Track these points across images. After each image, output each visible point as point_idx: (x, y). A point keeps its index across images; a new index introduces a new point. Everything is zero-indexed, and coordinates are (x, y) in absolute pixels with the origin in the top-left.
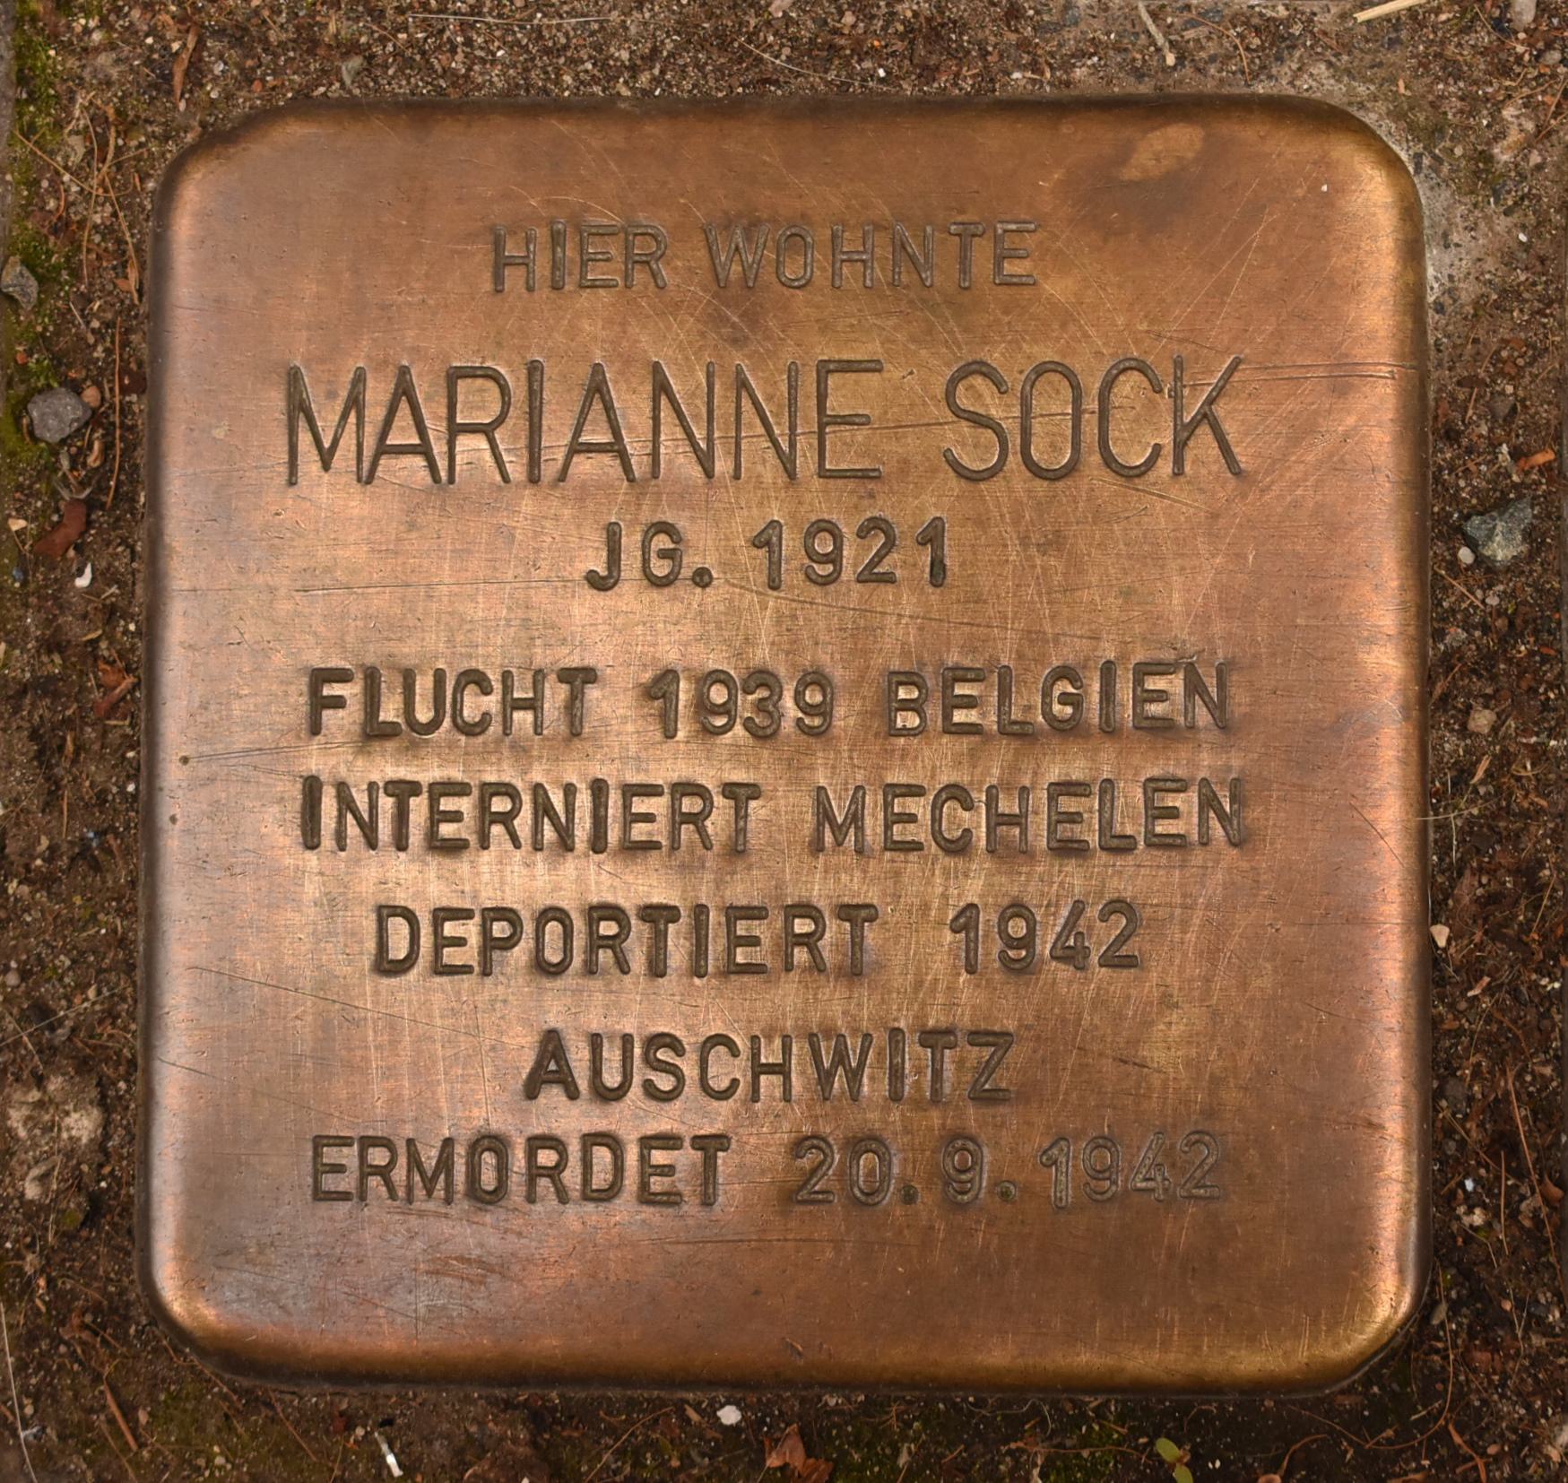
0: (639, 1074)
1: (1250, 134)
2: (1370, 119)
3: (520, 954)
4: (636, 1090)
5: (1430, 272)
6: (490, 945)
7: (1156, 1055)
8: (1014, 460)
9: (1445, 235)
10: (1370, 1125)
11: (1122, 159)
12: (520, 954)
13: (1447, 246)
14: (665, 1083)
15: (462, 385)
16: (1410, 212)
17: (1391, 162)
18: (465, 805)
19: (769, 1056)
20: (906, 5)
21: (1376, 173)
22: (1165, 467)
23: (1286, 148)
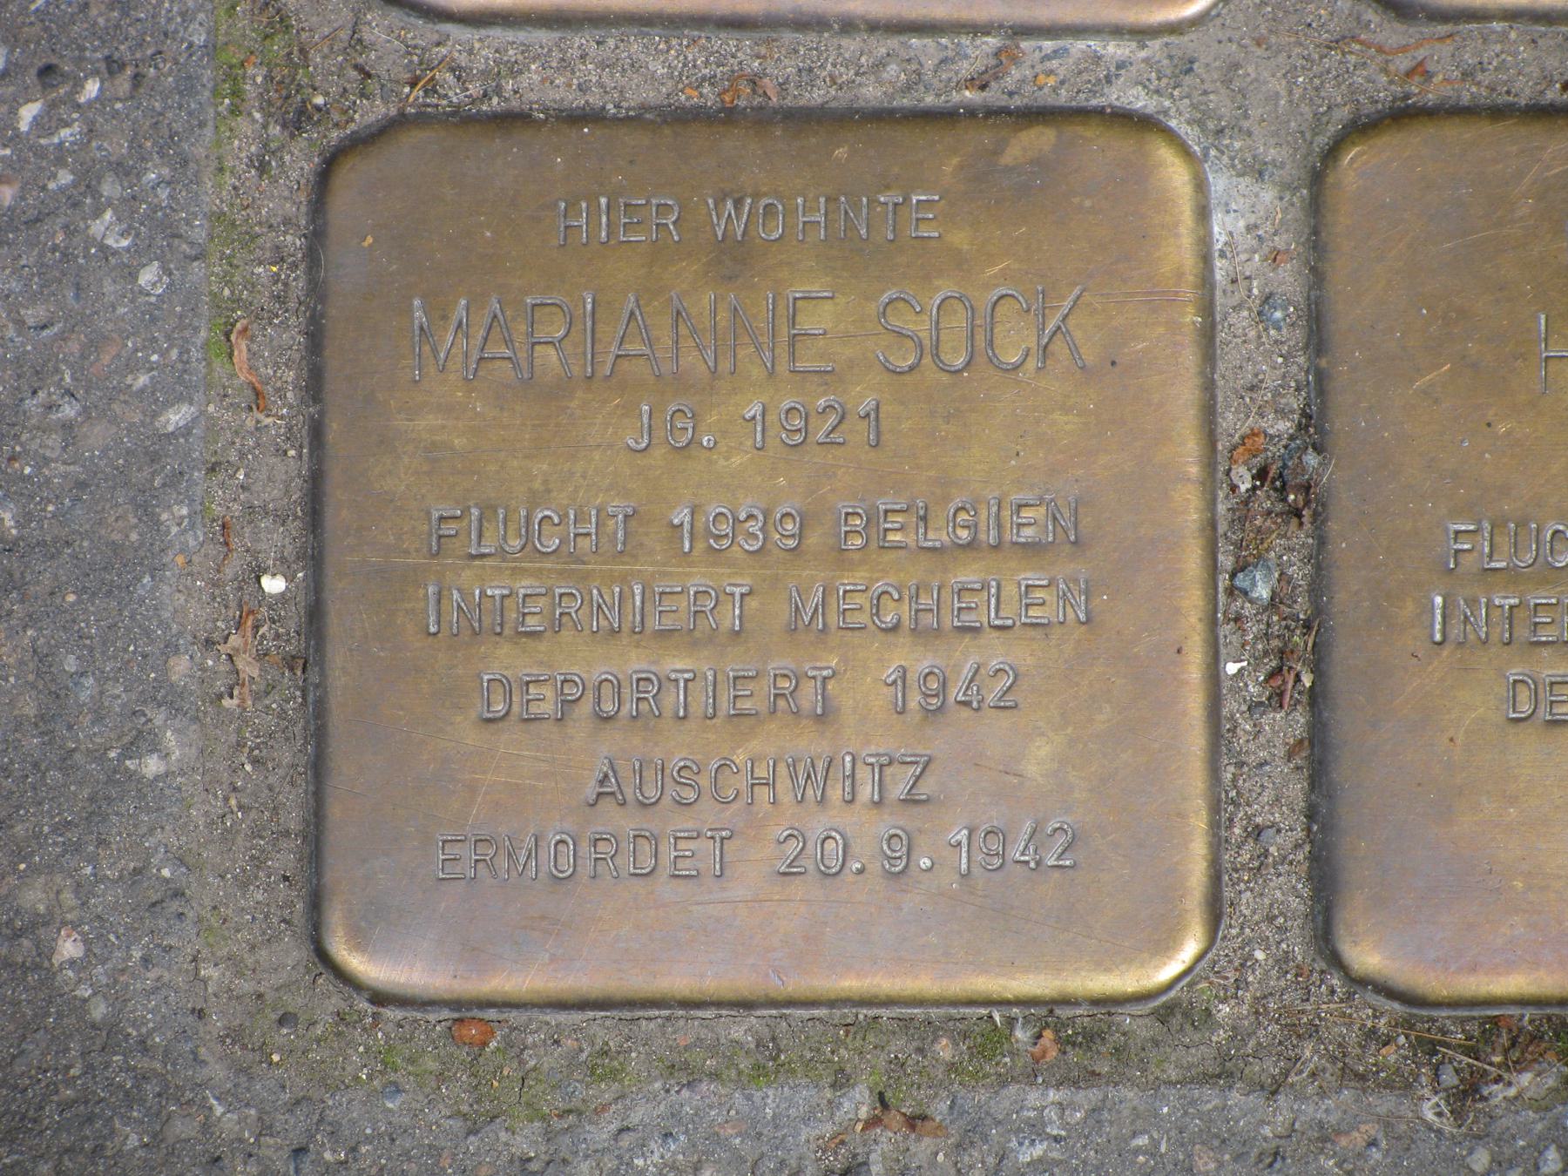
0: (670, 790)
1: (1090, 132)
2: (1173, 123)
3: (586, 707)
4: (667, 800)
5: (1216, 229)
6: (568, 704)
7: (1032, 769)
8: (927, 360)
9: (1227, 204)
10: (1179, 815)
11: (997, 152)
12: (586, 707)
13: (1228, 212)
14: (691, 795)
15: (537, 348)
16: (1201, 186)
17: (1185, 151)
18: (548, 691)
19: (761, 772)
20: (1311, 7)
21: (1177, 161)
22: (1032, 364)
23: (1100, 150)
